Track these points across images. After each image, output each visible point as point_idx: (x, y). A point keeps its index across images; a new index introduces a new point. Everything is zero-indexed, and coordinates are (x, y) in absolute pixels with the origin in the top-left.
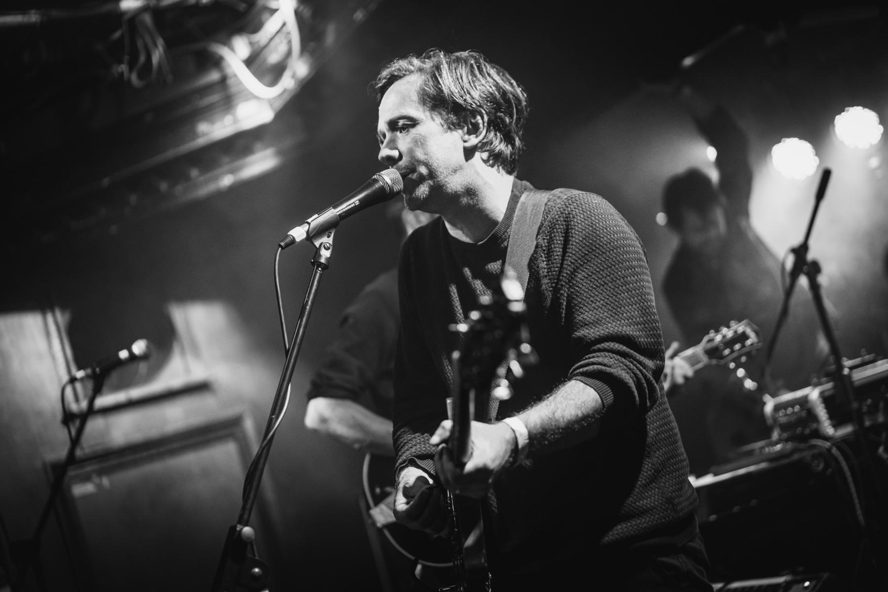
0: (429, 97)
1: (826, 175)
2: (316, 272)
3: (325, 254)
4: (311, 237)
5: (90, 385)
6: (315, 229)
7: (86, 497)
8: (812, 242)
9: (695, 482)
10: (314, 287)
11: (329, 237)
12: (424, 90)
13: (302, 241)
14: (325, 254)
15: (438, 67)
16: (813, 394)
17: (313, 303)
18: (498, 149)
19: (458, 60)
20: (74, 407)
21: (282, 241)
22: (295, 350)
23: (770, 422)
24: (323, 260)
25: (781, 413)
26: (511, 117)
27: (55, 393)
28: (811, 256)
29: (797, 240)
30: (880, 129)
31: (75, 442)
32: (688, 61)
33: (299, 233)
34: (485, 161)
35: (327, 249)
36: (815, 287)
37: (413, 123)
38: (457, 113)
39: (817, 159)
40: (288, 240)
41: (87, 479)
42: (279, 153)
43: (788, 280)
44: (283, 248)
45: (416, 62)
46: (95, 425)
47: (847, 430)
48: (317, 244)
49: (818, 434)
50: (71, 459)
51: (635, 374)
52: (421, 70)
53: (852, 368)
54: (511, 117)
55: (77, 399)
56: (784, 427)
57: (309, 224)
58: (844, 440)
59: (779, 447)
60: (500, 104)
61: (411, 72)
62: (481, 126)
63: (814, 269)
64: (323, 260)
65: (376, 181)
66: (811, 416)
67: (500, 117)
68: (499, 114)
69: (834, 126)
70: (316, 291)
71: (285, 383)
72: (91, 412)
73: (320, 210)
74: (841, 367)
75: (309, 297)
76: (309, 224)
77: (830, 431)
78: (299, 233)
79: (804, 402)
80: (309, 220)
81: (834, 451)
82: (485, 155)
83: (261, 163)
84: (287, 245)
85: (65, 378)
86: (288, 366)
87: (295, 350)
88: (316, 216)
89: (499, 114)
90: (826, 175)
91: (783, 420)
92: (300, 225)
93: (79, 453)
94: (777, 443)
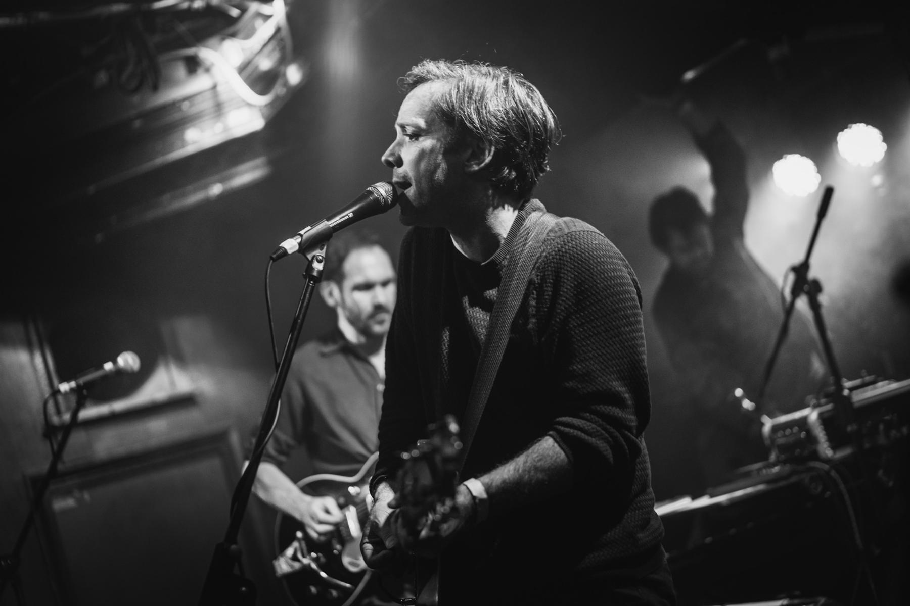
1: (829, 193)
4: (305, 247)
5: (73, 399)
7: (66, 512)
8: (813, 261)
16: (812, 415)
20: (55, 420)
21: (274, 253)
23: (767, 442)
25: (780, 434)
28: (812, 274)
30: (884, 147)
31: (57, 455)
32: (689, 75)
33: (291, 245)
35: (319, 261)
36: (815, 306)
39: (819, 176)
41: (68, 493)
46: (77, 438)
47: (840, 454)
48: (310, 257)
49: (815, 456)
50: (53, 473)
53: (852, 389)
55: (59, 412)
56: (782, 449)
58: (843, 461)
59: (776, 469)
64: (315, 274)
65: (371, 193)
66: (811, 439)
73: (313, 223)
74: (840, 388)
76: (301, 236)
77: (825, 449)
78: (291, 245)
79: (803, 423)
80: (302, 232)
81: (833, 473)
83: (247, 174)
84: (279, 257)
85: (47, 392)
88: (309, 228)
90: (829, 193)
91: (781, 441)
92: (292, 237)
93: (60, 467)
94: (774, 465)
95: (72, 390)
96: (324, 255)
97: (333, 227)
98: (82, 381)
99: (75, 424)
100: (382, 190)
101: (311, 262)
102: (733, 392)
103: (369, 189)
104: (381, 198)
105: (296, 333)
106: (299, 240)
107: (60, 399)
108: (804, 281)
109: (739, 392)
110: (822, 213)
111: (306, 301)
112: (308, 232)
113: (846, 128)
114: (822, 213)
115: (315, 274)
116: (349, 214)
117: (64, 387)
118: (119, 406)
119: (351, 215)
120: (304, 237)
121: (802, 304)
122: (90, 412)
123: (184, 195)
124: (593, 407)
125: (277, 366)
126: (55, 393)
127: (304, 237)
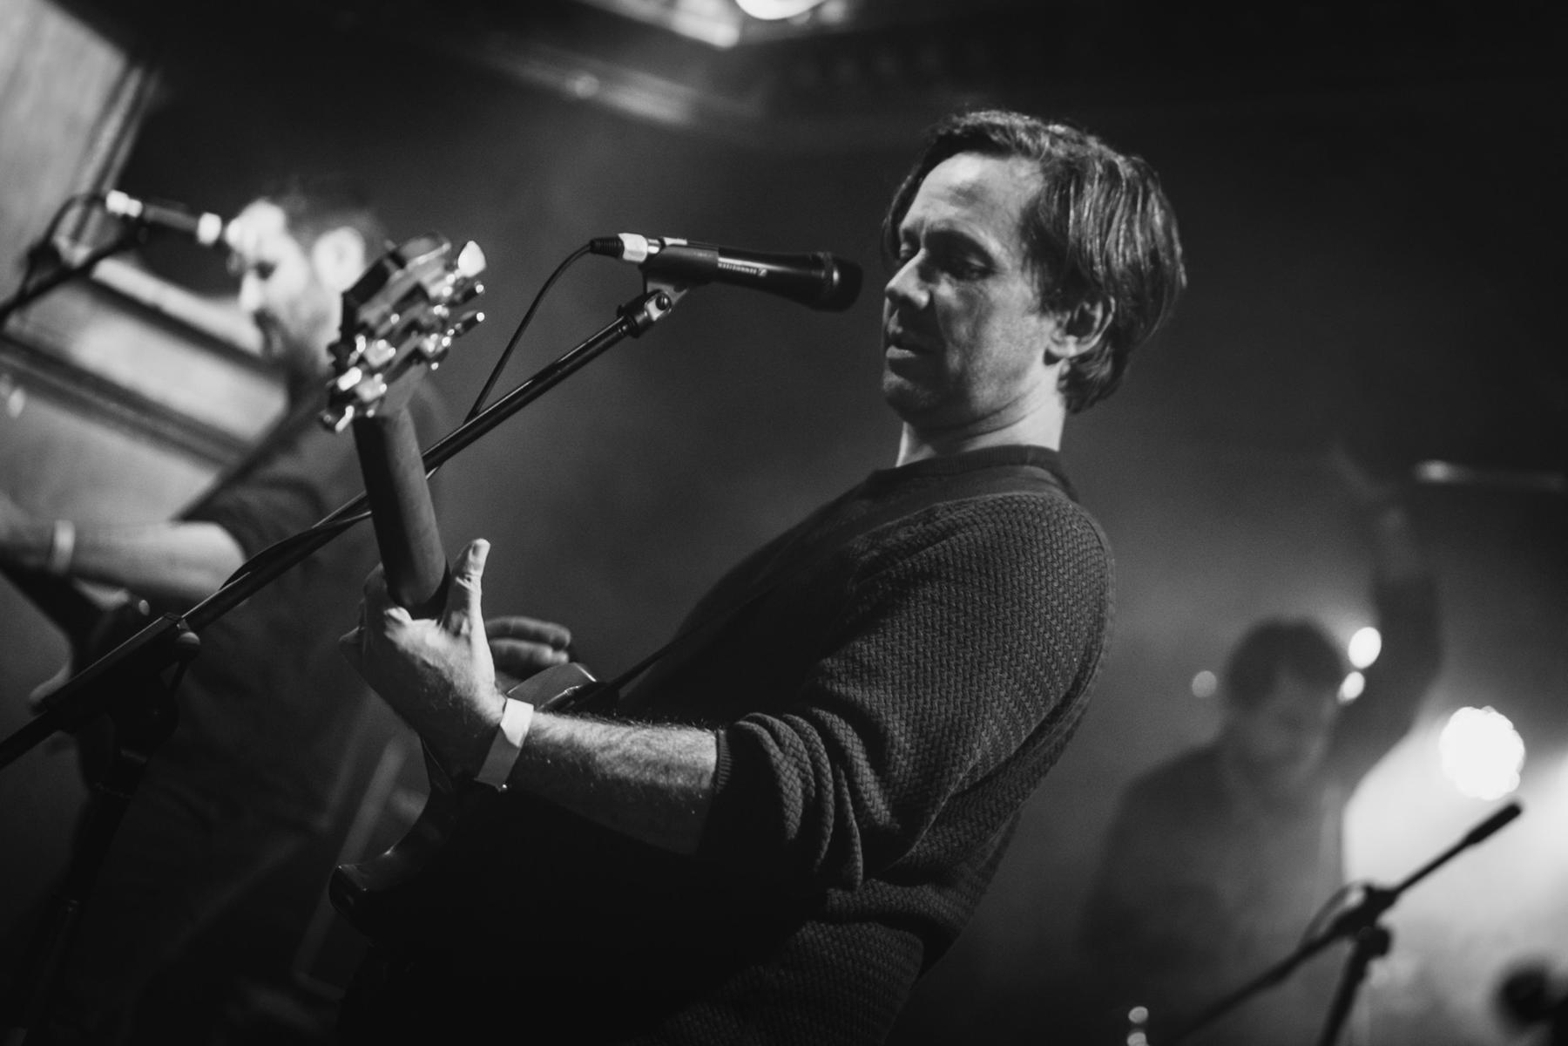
0: (942, 198)
1: (1509, 813)
4: (653, 267)
5: (111, 237)
13: (632, 263)
20: (62, 241)
27: (49, 195)
28: (1391, 918)
29: (1388, 878)
31: (23, 299)
32: (1436, 471)
35: (660, 306)
38: (1064, 277)
43: (1323, 929)
46: (66, 304)
51: (820, 786)
55: (76, 237)
57: (663, 245)
61: (1025, 152)
62: (1096, 325)
63: (1380, 943)
72: (82, 276)
76: (663, 245)
78: (637, 247)
80: (669, 241)
83: (650, 98)
85: (85, 187)
88: (683, 242)
90: (1509, 813)
92: (647, 236)
93: (13, 323)
95: (125, 218)
96: (674, 300)
98: (154, 213)
99: (82, 276)
101: (647, 297)
105: (540, 386)
106: (655, 250)
107: (96, 215)
108: (1365, 923)
109: (1138, 1014)
110: (1477, 836)
111: (593, 349)
114: (1477, 836)
115: (639, 319)
116: (763, 268)
117: (120, 203)
118: (176, 301)
119: (763, 272)
120: (665, 251)
121: (1345, 949)
122: (118, 273)
123: (1162, 207)
124: (815, 711)
125: (474, 413)
126: (96, 199)
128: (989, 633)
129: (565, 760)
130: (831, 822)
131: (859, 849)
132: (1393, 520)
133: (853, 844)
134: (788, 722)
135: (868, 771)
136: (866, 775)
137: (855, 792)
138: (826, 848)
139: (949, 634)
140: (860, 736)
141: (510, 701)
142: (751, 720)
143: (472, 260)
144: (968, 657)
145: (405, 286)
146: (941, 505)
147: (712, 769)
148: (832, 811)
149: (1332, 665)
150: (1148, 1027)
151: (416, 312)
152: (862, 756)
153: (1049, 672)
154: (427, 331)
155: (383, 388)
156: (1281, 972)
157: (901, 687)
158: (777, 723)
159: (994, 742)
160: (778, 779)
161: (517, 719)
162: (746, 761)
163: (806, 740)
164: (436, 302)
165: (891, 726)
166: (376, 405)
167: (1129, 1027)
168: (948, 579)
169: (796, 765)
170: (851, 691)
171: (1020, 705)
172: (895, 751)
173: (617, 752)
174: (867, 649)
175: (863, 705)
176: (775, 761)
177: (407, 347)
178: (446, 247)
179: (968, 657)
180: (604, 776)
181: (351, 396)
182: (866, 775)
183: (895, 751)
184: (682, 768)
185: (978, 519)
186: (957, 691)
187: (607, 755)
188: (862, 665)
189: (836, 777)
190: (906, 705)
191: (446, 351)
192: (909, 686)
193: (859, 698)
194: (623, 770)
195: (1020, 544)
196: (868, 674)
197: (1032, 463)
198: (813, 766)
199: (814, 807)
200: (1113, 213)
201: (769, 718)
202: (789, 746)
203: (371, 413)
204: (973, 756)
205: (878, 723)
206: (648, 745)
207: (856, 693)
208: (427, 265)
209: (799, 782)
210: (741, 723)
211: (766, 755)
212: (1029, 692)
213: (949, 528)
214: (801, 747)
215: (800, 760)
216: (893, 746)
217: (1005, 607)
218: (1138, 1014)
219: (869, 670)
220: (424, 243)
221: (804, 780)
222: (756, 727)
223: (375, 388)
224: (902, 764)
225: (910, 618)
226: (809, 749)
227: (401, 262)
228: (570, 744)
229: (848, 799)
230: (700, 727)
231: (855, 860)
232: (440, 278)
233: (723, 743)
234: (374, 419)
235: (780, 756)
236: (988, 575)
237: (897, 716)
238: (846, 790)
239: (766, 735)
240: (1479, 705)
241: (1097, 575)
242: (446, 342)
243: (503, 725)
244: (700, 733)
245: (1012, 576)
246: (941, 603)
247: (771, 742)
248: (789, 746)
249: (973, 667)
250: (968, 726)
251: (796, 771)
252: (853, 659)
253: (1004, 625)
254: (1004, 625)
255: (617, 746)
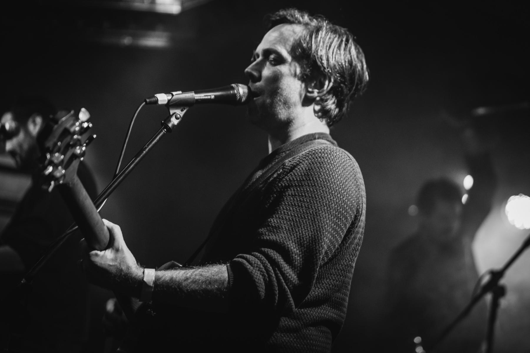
2: (162, 131)
3: (174, 121)
4: (171, 104)
6: (175, 100)
8: (509, 273)
9: (51, 188)
10: (155, 141)
11: (182, 111)
12: (300, 41)
14: (174, 121)
15: (318, 29)
17: (149, 150)
18: (329, 107)
19: (335, 32)
21: (148, 98)
22: (121, 178)
24: (170, 125)
26: (350, 90)
28: (503, 281)
29: (498, 266)
32: (481, 111)
33: (163, 98)
34: (315, 112)
35: (177, 118)
37: (280, 60)
38: (313, 72)
40: (153, 99)
42: (172, 39)
43: (479, 291)
44: (146, 103)
45: (306, 18)
48: (172, 112)
51: (270, 276)
52: (306, 24)
54: (350, 90)
60: (348, 75)
61: (299, 23)
64: (170, 125)
65: (233, 88)
67: (342, 87)
68: (342, 85)
69: (506, 203)
70: (156, 143)
71: (104, 197)
73: (184, 91)
75: (148, 146)
76: (173, 95)
78: (163, 98)
80: (174, 93)
82: (317, 108)
83: (156, 41)
84: (151, 103)
86: (111, 186)
87: (121, 178)
88: (180, 92)
89: (342, 85)
92: (166, 93)
96: (182, 115)
97: (197, 100)
100: (242, 90)
102: (414, 338)
103: (234, 85)
104: (238, 95)
106: (170, 97)
112: (178, 95)
113: (517, 195)
119: (213, 97)
121: (489, 297)
127: (174, 97)
128: (316, 201)
129: (171, 287)
130: (277, 288)
131: (290, 296)
132: (469, 133)
133: (287, 295)
134: (252, 255)
135: (286, 265)
136: (286, 268)
137: (283, 274)
138: (277, 299)
139: (302, 206)
140: (279, 253)
141: (145, 269)
142: (238, 257)
143: (84, 115)
144: (311, 212)
145: (61, 130)
146: (287, 161)
147: (227, 279)
148: (276, 284)
149: (455, 191)
150: (422, 344)
151: (68, 139)
152: (282, 260)
153: (344, 208)
154: (74, 146)
155: (64, 171)
156: (467, 311)
157: (289, 230)
158: (248, 256)
159: (330, 240)
160: (253, 277)
161: (150, 275)
162: (238, 272)
163: (260, 260)
164: (74, 133)
165: (289, 246)
166: (63, 178)
167: (415, 345)
168: (296, 185)
169: (259, 270)
170: (271, 237)
171: (336, 223)
172: (294, 255)
173: (189, 281)
174: (273, 221)
175: (277, 241)
176: (250, 270)
177: (69, 154)
178: (72, 112)
179: (311, 212)
180: (187, 290)
181: (51, 176)
182: (286, 268)
183: (294, 255)
184: (216, 281)
185: (301, 161)
186: (310, 226)
187: (186, 282)
188: (273, 227)
189: (275, 271)
190: (293, 237)
191: (84, 152)
192: (292, 229)
193: (275, 239)
194: (194, 286)
195: (319, 165)
196: (276, 229)
197: (318, 138)
198: (265, 269)
199: (269, 284)
200: (331, 43)
201: (245, 255)
202: (254, 263)
203: (61, 182)
204: (323, 248)
205: (285, 246)
206: (201, 275)
207: (273, 237)
208: (66, 120)
209: (261, 276)
210: (235, 259)
211: (246, 269)
212: (338, 218)
213: (291, 167)
214: (259, 263)
215: (260, 268)
216: (293, 253)
217: (319, 190)
218: (417, 340)
219: (276, 227)
220: (64, 113)
221: (263, 275)
222: (240, 260)
223: (61, 172)
224: (298, 259)
225: (285, 205)
226: (262, 263)
227: (56, 121)
228: (172, 279)
229: (281, 278)
230: (220, 264)
231: (290, 301)
232: (74, 124)
233: (229, 268)
234: (63, 184)
235: (252, 268)
236: (310, 180)
237: (291, 242)
238: (280, 275)
239: (245, 261)
240: (517, 194)
241: (351, 169)
242: (84, 148)
243: (145, 280)
244: (220, 266)
245: (319, 177)
246: (295, 195)
247: (247, 264)
248: (254, 263)
249: (314, 215)
250: (318, 237)
251: (259, 272)
252: (269, 226)
253: (321, 196)
254: (321, 196)
255: (190, 278)
